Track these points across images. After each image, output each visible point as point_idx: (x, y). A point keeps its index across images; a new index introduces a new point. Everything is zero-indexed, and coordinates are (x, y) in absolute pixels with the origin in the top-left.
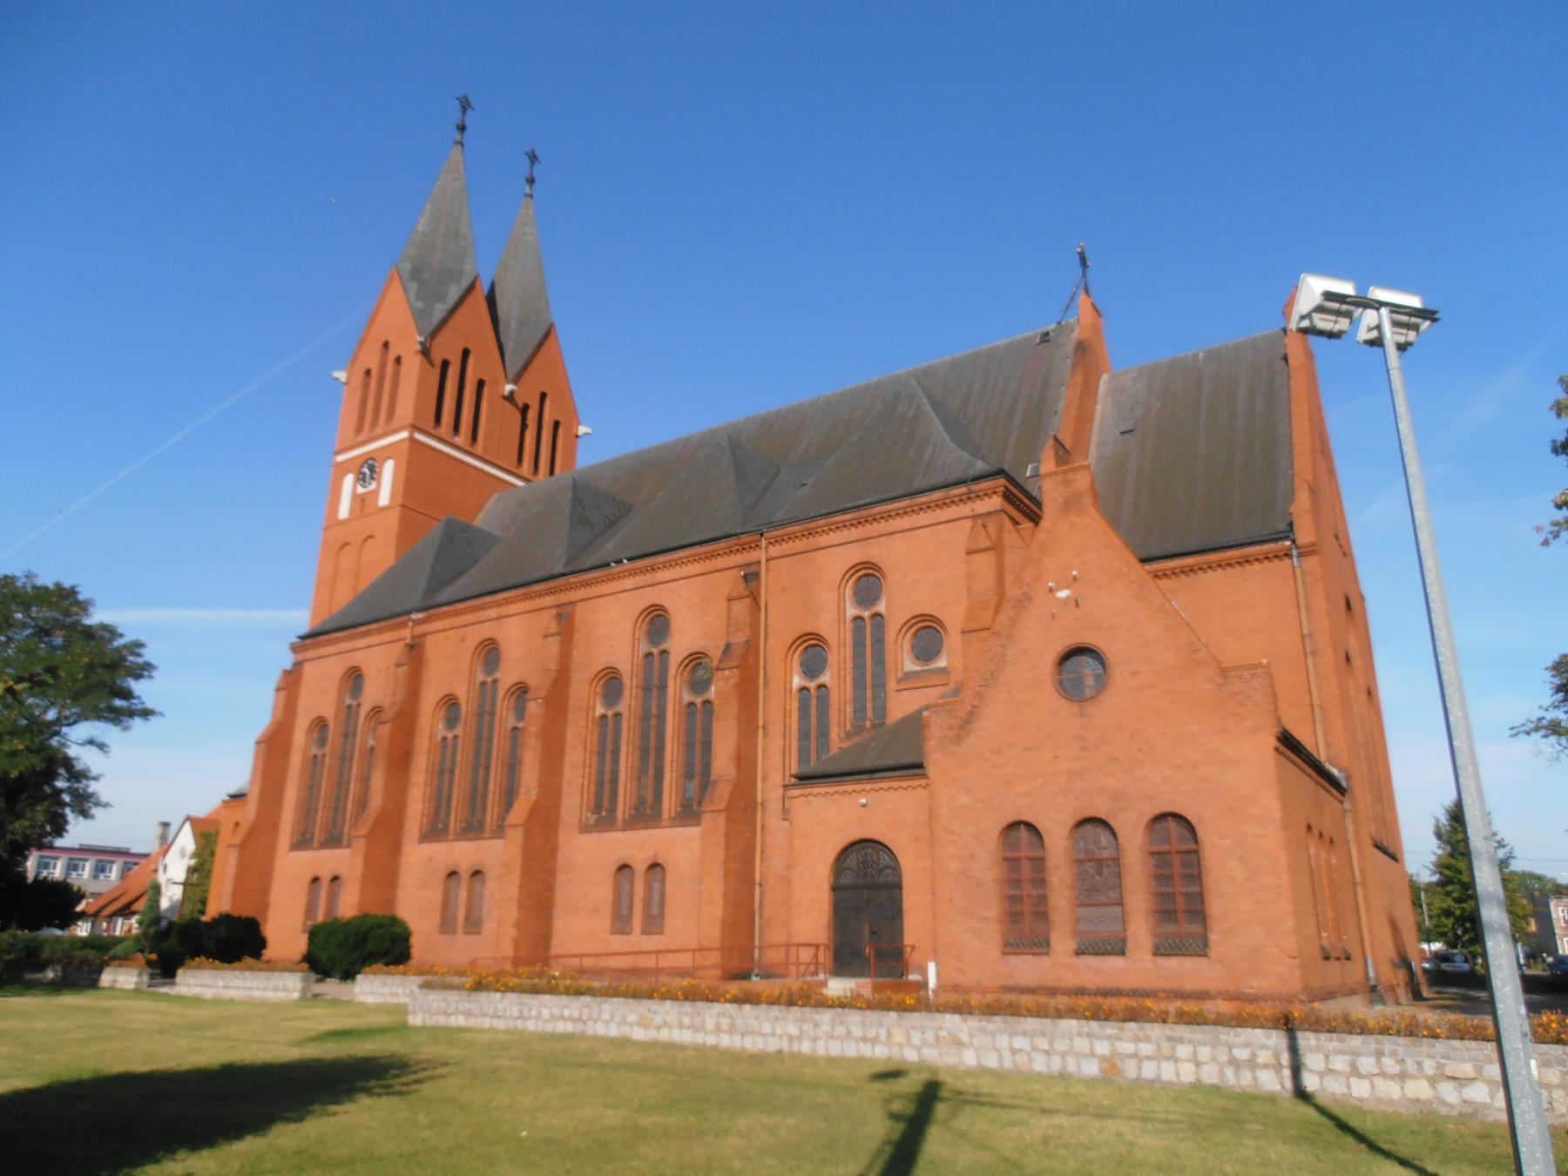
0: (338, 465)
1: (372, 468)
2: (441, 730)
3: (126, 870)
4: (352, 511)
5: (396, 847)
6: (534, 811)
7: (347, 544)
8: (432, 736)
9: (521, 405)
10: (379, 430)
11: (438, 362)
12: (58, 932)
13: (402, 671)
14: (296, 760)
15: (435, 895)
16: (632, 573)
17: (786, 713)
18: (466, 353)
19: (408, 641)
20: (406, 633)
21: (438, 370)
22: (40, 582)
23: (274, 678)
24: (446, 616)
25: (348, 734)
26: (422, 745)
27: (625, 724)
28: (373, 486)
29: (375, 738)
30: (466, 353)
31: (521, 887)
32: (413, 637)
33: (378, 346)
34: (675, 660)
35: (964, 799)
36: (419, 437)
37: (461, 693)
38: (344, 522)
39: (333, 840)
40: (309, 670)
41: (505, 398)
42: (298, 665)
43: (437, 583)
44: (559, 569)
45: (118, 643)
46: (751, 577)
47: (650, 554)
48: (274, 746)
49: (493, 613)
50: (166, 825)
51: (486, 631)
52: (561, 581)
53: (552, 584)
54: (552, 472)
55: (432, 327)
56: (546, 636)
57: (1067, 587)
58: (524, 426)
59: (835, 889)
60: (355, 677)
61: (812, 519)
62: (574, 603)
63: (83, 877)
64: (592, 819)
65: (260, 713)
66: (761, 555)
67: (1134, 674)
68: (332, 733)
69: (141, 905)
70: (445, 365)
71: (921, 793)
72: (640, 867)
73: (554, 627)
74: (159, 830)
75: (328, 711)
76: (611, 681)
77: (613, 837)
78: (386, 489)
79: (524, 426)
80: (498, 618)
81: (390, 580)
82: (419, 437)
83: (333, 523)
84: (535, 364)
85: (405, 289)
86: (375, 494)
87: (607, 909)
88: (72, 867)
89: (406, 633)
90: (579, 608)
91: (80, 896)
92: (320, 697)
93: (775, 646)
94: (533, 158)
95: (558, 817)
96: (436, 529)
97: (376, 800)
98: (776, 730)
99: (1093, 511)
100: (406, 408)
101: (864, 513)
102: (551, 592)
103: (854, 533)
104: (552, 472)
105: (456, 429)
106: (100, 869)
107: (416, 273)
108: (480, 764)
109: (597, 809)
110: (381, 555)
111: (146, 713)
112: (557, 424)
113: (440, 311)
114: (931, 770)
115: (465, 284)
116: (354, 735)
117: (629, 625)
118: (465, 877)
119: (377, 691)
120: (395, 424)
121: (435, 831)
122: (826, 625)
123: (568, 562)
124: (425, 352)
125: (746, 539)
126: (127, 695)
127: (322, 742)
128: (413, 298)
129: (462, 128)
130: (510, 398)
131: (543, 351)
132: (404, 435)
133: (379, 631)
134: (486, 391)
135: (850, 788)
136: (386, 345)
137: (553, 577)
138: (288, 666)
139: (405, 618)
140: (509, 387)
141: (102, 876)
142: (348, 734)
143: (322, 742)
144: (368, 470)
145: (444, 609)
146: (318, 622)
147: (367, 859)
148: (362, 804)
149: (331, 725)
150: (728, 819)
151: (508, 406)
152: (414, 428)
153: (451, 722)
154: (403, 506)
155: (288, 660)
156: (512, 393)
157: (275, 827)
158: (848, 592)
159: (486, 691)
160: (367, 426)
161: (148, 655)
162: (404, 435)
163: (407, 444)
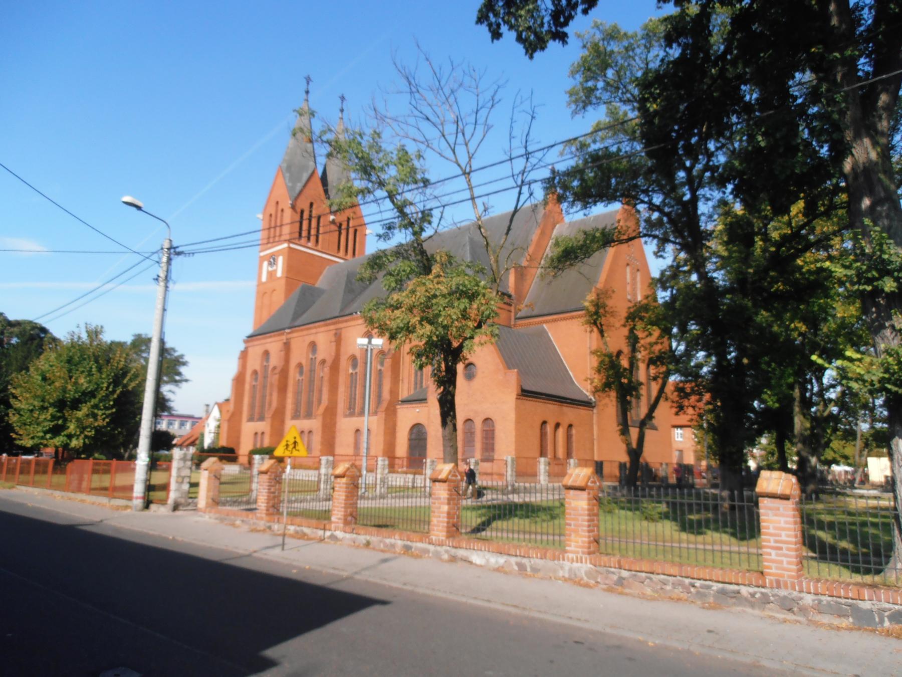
0: (261, 257)
1: (274, 259)
2: (298, 377)
3: (193, 424)
4: (267, 278)
5: (283, 422)
7: (265, 293)
11: (299, 211)
12: (166, 452)
13: (283, 353)
14: (247, 387)
19: (285, 341)
20: (284, 338)
24: (297, 331)
25: (265, 377)
27: (358, 377)
28: (275, 268)
29: (274, 379)
31: (322, 438)
32: (287, 339)
33: (274, 204)
36: (292, 246)
37: (304, 362)
38: (265, 283)
40: (250, 350)
42: (246, 348)
43: (297, 315)
44: (337, 314)
45: (176, 354)
48: (239, 381)
49: (314, 331)
50: (208, 405)
51: (312, 338)
52: (337, 319)
53: (334, 320)
55: (295, 195)
56: (331, 342)
59: (410, 440)
60: (266, 354)
62: (341, 329)
64: (348, 412)
65: (233, 368)
67: (483, 372)
69: (197, 442)
70: (302, 212)
71: (426, 409)
73: (333, 339)
74: (205, 408)
75: (258, 367)
78: (280, 271)
80: (316, 333)
81: (281, 311)
82: (292, 246)
83: (260, 284)
85: (284, 177)
86: (275, 271)
87: (352, 445)
89: (284, 338)
90: (343, 330)
91: (173, 437)
92: (254, 363)
94: (343, 98)
96: (298, 289)
97: (275, 404)
98: (406, 381)
106: (182, 424)
107: (289, 168)
108: (311, 391)
109: (350, 409)
110: (279, 299)
111: (186, 381)
113: (299, 186)
115: (310, 172)
118: (306, 433)
119: (275, 360)
121: (296, 416)
123: (342, 310)
124: (293, 207)
126: (179, 374)
127: (256, 379)
128: (287, 181)
129: (307, 92)
130: (333, 222)
132: (285, 245)
135: (414, 405)
136: (277, 203)
138: (242, 348)
139: (282, 331)
141: (183, 428)
143: (256, 379)
144: (272, 259)
145: (297, 328)
146: (265, 316)
147: (272, 426)
148: (270, 404)
149: (259, 373)
150: (386, 414)
153: (301, 373)
154: (287, 277)
155: (242, 347)
157: (241, 413)
159: (313, 361)
161: (186, 359)
162: (285, 245)
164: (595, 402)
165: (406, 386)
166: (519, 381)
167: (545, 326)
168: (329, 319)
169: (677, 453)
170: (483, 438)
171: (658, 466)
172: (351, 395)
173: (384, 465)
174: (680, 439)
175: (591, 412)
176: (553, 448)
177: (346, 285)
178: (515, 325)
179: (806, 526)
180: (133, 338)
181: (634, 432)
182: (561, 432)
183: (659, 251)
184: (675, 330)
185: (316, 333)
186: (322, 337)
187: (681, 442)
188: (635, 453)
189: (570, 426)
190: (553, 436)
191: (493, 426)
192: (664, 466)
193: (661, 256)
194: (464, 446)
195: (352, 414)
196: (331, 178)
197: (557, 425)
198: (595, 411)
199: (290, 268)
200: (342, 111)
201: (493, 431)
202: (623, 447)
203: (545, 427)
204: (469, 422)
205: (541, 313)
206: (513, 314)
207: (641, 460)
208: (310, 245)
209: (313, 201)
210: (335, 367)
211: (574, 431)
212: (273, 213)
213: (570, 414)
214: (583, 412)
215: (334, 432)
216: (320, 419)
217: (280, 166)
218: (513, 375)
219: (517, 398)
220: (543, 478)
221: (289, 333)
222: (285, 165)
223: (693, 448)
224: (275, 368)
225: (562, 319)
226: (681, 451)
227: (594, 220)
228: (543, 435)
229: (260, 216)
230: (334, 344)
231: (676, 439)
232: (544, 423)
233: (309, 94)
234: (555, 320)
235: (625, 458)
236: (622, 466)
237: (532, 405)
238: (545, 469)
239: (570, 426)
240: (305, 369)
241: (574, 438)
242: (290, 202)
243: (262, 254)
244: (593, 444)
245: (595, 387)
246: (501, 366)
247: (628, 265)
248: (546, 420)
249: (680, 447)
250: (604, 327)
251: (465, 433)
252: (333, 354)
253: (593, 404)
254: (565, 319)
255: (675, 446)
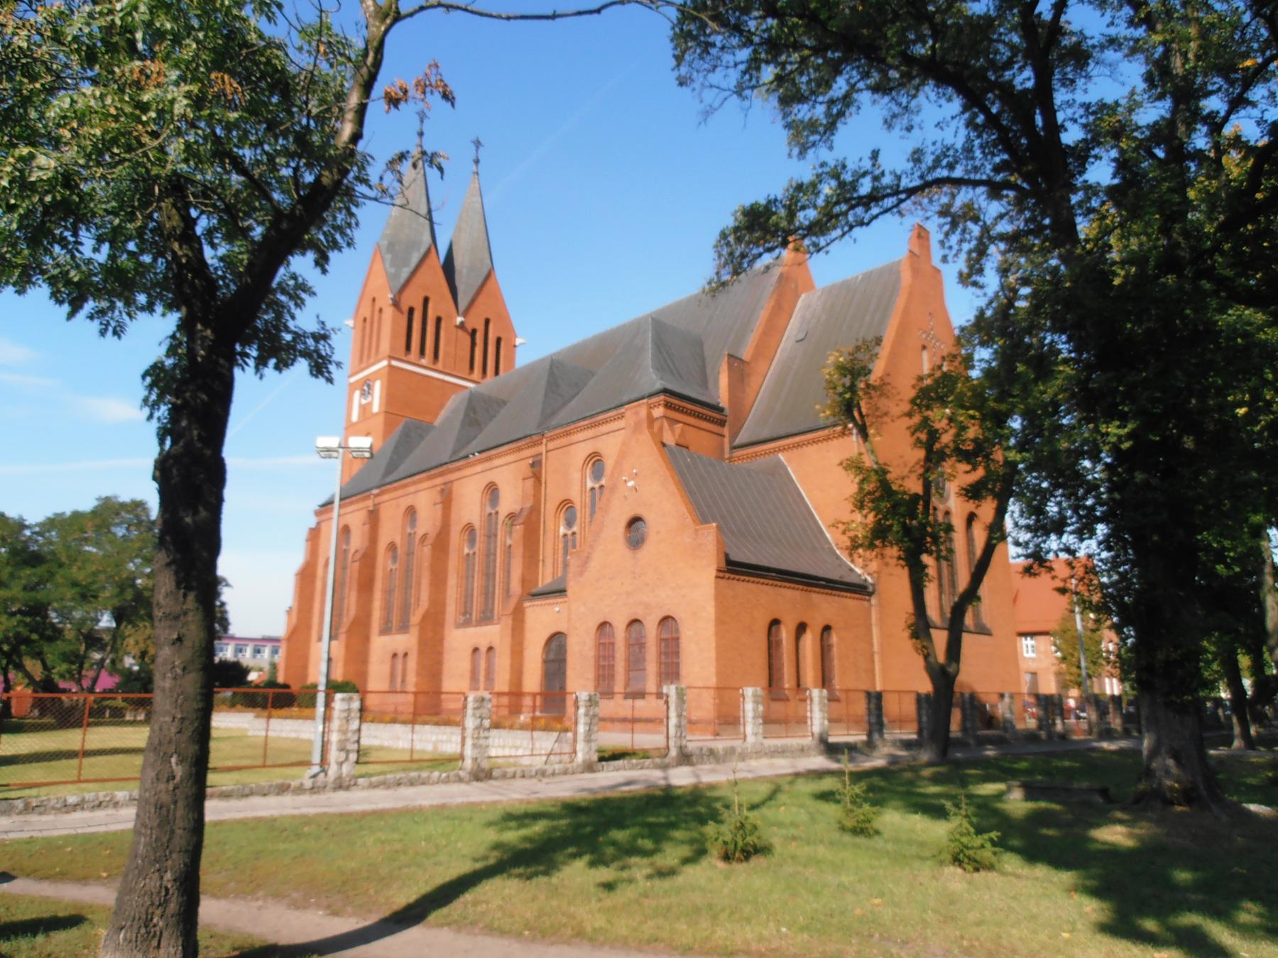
0: (351, 385)
1: (369, 386)
2: (391, 566)
5: (366, 639)
6: (425, 617)
8: (385, 568)
9: (470, 330)
10: (372, 360)
11: (405, 309)
13: (367, 527)
15: (386, 668)
16: (480, 461)
17: (555, 552)
18: (426, 300)
20: (369, 504)
21: (406, 316)
22: (121, 500)
23: (304, 534)
26: (379, 574)
28: (369, 399)
30: (426, 300)
34: (502, 516)
35: (582, 609)
36: (394, 363)
37: (398, 541)
39: (404, 628)
41: (457, 327)
42: (319, 523)
43: (392, 466)
46: (536, 465)
47: (592, 418)
49: (412, 489)
52: (445, 468)
53: (440, 469)
54: (497, 373)
57: (633, 479)
58: (473, 344)
61: (568, 424)
63: (247, 658)
64: (462, 619)
66: (542, 449)
68: (479, 533)
70: (411, 311)
72: (483, 649)
73: (439, 499)
76: (470, 529)
77: (471, 631)
78: (376, 401)
79: (473, 344)
82: (394, 363)
84: (481, 299)
85: (383, 260)
86: (370, 404)
87: (468, 675)
88: (239, 650)
89: (369, 504)
90: (456, 486)
93: (549, 507)
94: (478, 144)
95: (444, 619)
98: (549, 562)
99: (646, 432)
100: (385, 346)
101: (593, 420)
102: (441, 474)
103: (590, 433)
104: (497, 373)
105: (422, 352)
106: (257, 651)
107: (391, 246)
112: (499, 340)
114: (569, 592)
115: (423, 250)
116: (496, 536)
117: (479, 495)
119: (357, 541)
120: (380, 356)
121: (385, 631)
122: (575, 494)
123: (455, 452)
124: (396, 304)
125: (535, 438)
130: (462, 326)
131: (485, 289)
133: (357, 501)
134: (443, 325)
135: (551, 601)
136: (374, 300)
137: (441, 465)
140: (459, 319)
141: (258, 656)
142: (491, 536)
143: (472, 541)
147: (348, 647)
151: (460, 333)
152: (391, 358)
153: (472, 541)
156: (462, 323)
158: (588, 471)
160: (365, 358)
162: (385, 363)
163: (386, 370)
164: (873, 585)
165: (549, 569)
166: (720, 543)
167: (781, 456)
168: (436, 467)
169: (1028, 677)
170: (660, 654)
171: (994, 698)
172: (466, 590)
173: (349, 710)
174: (1031, 655)
175: (866, 603)
176: (793, 670)
177: (466, 415)
178: (730, 459)
179: (951, 670)
180: (95, 503)
181: (940, 639)
182: (809, 642)
183: (969, 275)
184: (1016, 423)
185: (416, 492)
186: (424, 497)
187: (1033, 659)
188: (944, 677)
189: (827, 629)
190: (792, 647)
191: (677, 631)
192: (1007, 700)
193: (975, 284)
194: (628, 670)
195: (467, 623)
196: (459, 261)
197: (801, 628)
198: (874, 601)
199: (390, 398)
200: (477, 162)
201: (678, 639)
202: (919, 661)
203: (778, 630)
204: (636, 626)
205: (775, 435)
206: (726, 440)
207: (956, 689)
208: (424, 361)
209: (428, 294)
210: (441, 543)
211: (834, 639)
212: (368, 316)
213: (825, 607)
214: (850, 603)
215: (440, 653)
216: (414, 631)
217: (378, 245)
218: (709, 535)
219: (717, 577)
220: (751, 727)
221: (378, 495)
222: (384, 243)
223: (1054, 668)
224: (425, 536)
225: (809, 443)
226: (1034, 674)
227: (863, 280)
228: (772, 646)
229: (350, 323)
230: (439, 507)
231: (1025, 655)
232: (775, 622)
233: (424, 138)
234: (798, 445)
235: (926, 687)
236: (920, 700)
237: (746, 589)
238: (755, 710)
239: (827, 629)
240: (399, 551)
241: (835, 651)
242: (390, 296)
243: (353, 380)
244: (873, 662)
245: (853, 539)
246: (689, 520)
247: (924, 347)
248: (777, 616)
249: (1033, 666)
250: (868, 421)
251: (629, 645)
252: (438, 524)
253: (871, 589)
254: (815, 441)
255: (1023, 666)
